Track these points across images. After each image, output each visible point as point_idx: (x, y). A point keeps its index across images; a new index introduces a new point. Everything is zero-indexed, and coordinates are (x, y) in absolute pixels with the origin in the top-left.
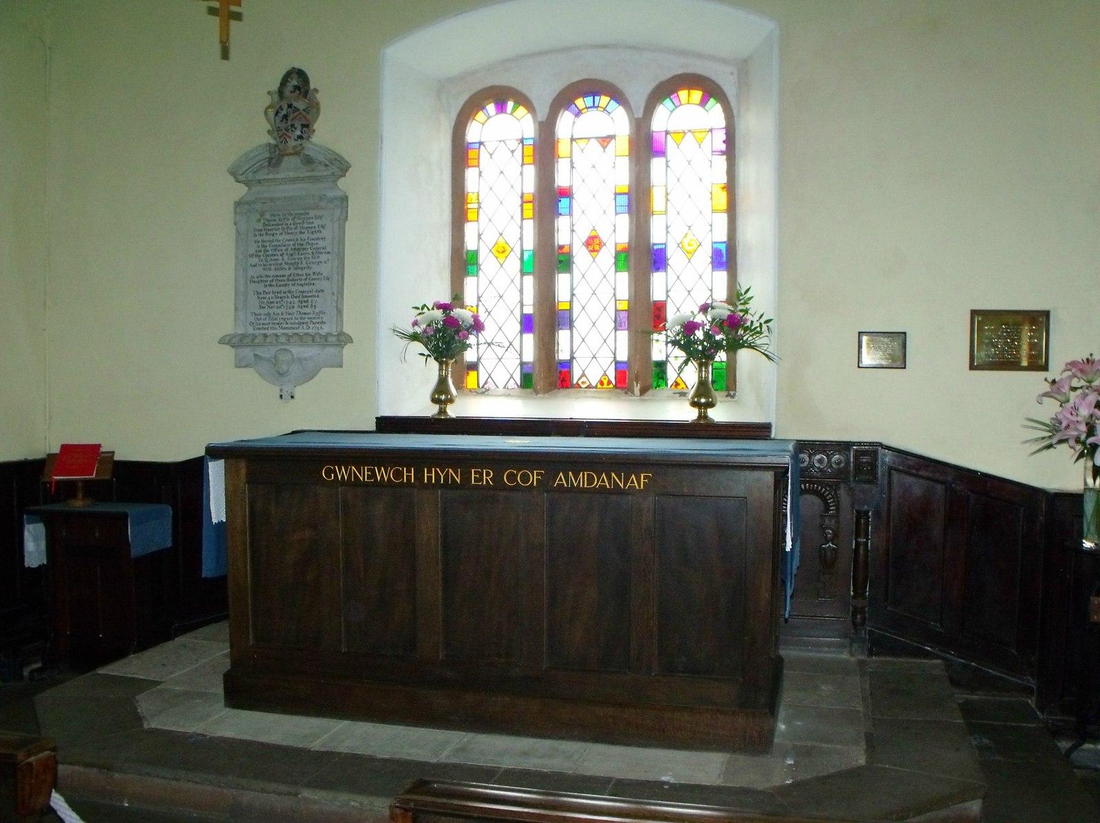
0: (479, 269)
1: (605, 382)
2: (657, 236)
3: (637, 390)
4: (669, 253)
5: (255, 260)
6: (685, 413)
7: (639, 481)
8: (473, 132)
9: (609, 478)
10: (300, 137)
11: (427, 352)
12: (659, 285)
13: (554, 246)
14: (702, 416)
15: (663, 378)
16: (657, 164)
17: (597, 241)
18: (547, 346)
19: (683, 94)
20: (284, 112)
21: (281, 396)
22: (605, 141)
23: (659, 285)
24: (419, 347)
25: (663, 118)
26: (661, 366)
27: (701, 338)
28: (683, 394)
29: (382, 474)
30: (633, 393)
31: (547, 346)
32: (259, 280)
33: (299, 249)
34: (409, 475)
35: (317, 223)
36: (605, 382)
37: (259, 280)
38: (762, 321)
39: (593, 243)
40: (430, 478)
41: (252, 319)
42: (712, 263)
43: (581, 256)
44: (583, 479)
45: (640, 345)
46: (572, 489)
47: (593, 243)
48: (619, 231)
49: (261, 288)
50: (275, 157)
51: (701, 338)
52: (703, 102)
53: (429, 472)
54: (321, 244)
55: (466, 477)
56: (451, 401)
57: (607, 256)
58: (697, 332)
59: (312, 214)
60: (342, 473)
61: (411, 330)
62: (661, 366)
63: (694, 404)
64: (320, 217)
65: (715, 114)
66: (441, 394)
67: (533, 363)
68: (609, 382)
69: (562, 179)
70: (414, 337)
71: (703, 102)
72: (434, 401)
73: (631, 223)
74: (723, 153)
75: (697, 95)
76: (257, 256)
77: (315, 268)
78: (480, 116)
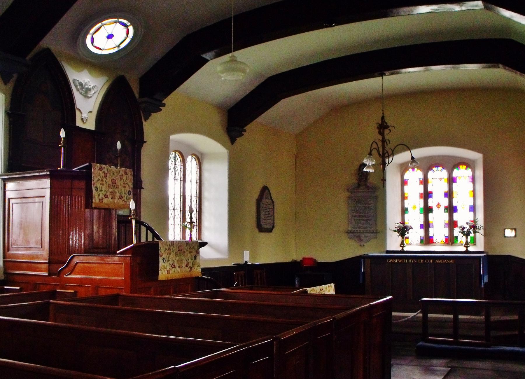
0: (408, 212)
1: (442, 241)
2: (455, 204)
3: (450, 243)
4: (458, 208)
5: (354, 211)
6: (464, 249)
7: (452, 261)
8: (406, 177)
9: (446, 261)
10: (365, 181)
11: (399, 235)
12: (456, 217)
13: (428, 207)
14: (467, 249)
15: (457, 240)
16: (454, 184)
17: (439, 205)
18: (427, 232)
19: (461, 166)
20: (360, 175)
21: (361, 246)
22: (441, 179)
23: (456, 216)
24: (397, 233)
25: (456, 173)
26: (457, 237)
27: (466, 231)
28: (462, 244)
29: (400, 261)
30: (449, 244)
31: (427, 232)
32: (355, 216)
33: (365, 209)
34: (406, 261)
35: (370, 202)
36: (442, 241)
37: (355, 216)
38: (481, 226)
39: (438, 205)
40: (410, 261)
41: (353, 226)
42: (469, 210)
43: (435, 209)
44: (441, 261)
45: (451, 232)
46: (439, 263)
47: (438, 205)
48: (445, 202)
49: (355, 218)
50: (359, 186)
51: (466, 231)
52: (466, 168)
53: (410, 260)
54: (371, 208)
55: (417, 261)
56: (405, 246)
57: (442, 208)
58: (465, 229)
59: (368, 200)
60: (391, 261)
61: (395, 229)
62: (457, 237)
63: (465, 246)
64: (371, 201)
65: (469, 172)
66: (402, 245)
67: (423, 237)
68: (443, 241)
69: (430, 189)
70: (395, 231)
71: (466, 168)
72: (401, 246)
73: (448, 200)
74: (471, 182)
75: (465, 167)
76: (354, 210)
77: (370, 214)
78: (408, 172)
